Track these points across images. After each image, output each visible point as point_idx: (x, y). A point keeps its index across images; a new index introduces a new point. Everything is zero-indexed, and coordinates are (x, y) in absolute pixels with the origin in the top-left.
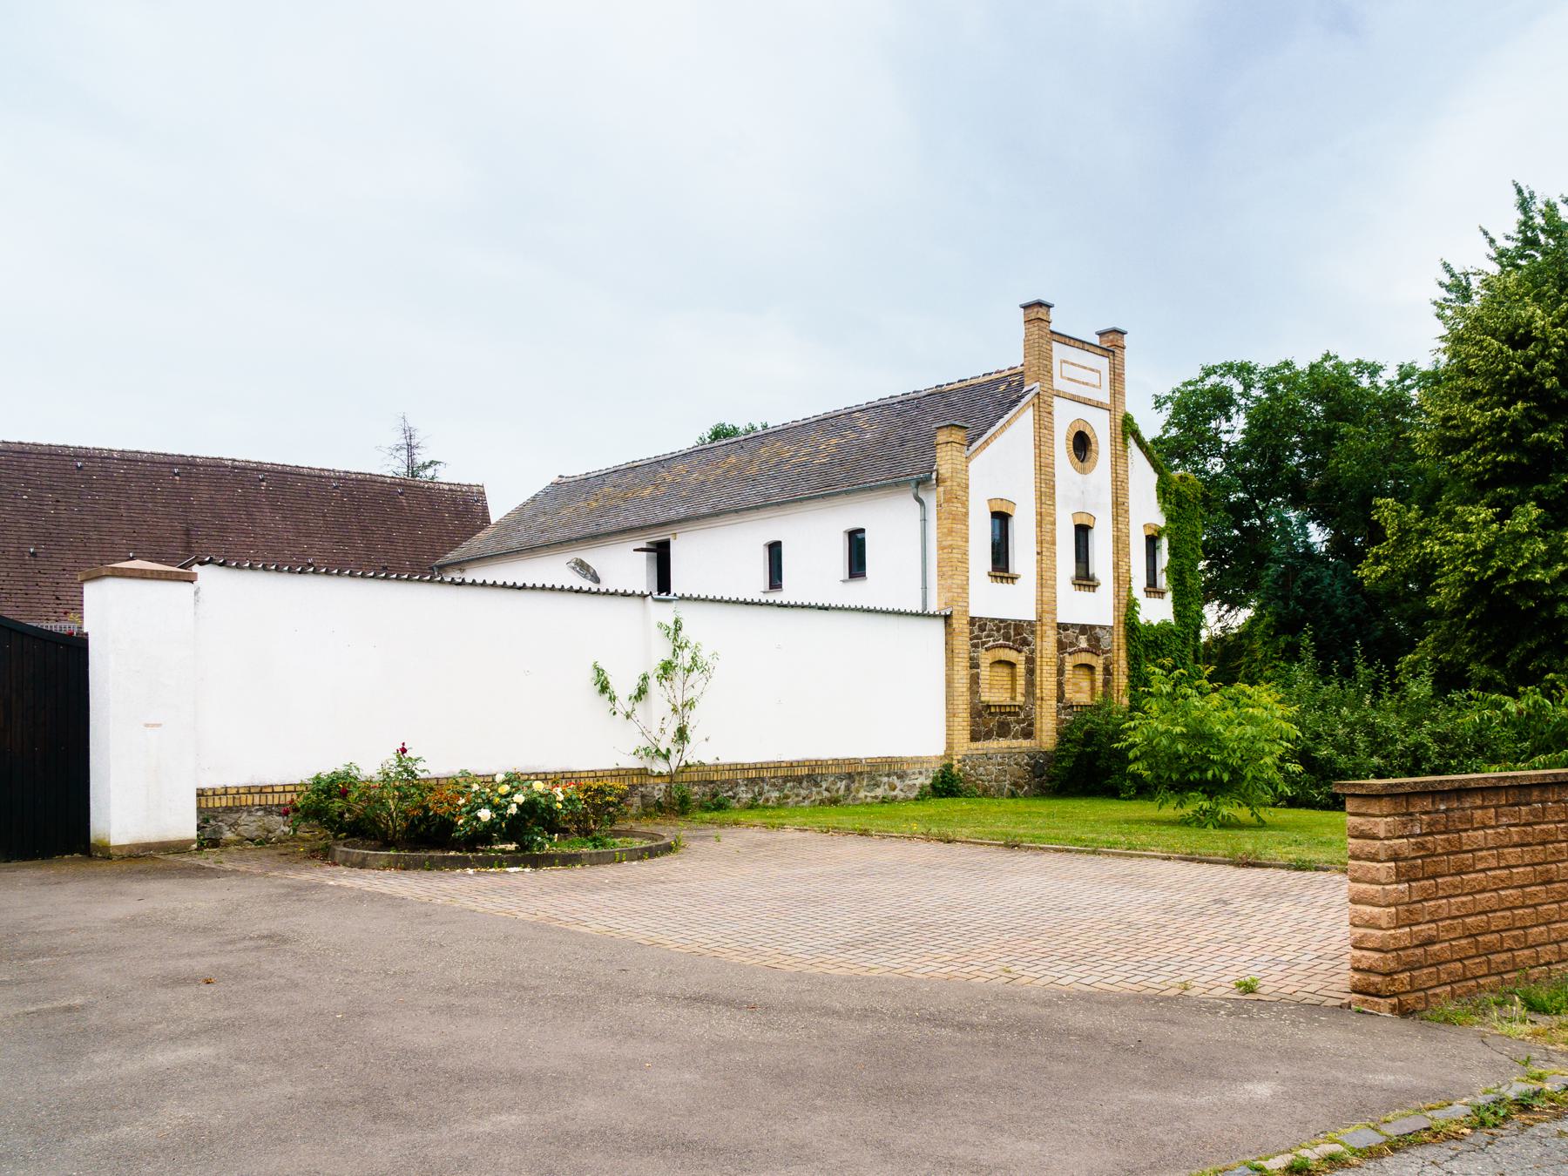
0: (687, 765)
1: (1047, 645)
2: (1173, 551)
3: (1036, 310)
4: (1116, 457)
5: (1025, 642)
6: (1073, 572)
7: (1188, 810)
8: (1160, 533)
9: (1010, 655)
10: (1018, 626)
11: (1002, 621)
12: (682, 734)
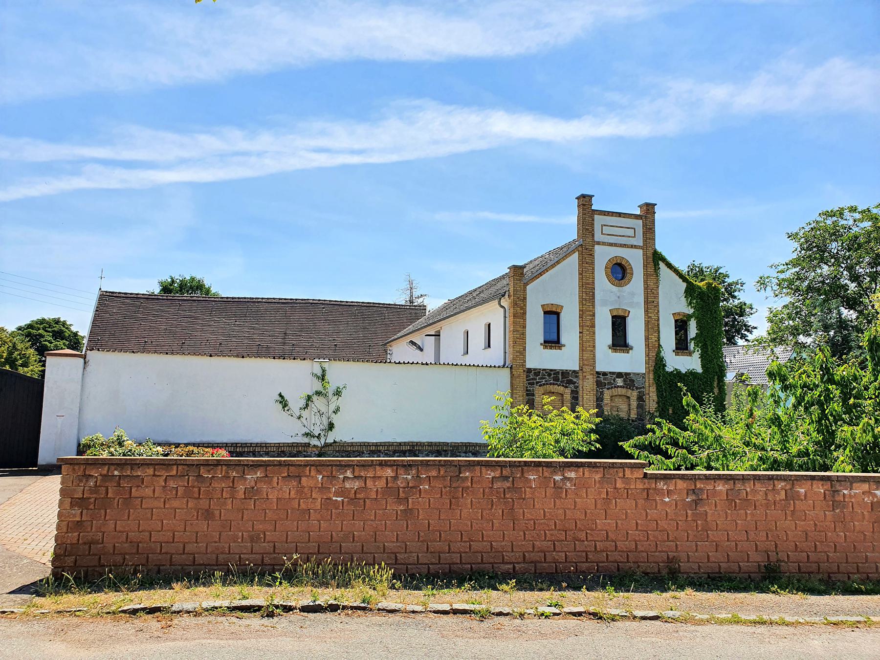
0: (335, 442)
1: (587, 386)
2: (699, 326)
3: (585, 201)
4: (647, 276)
5: (571, 382)
6: (610, 341)
7: (733, 401)
8: (689, 317)
9: (561, 389)
10: (565, 373)
11: (551, 370)
12: (331, 426)
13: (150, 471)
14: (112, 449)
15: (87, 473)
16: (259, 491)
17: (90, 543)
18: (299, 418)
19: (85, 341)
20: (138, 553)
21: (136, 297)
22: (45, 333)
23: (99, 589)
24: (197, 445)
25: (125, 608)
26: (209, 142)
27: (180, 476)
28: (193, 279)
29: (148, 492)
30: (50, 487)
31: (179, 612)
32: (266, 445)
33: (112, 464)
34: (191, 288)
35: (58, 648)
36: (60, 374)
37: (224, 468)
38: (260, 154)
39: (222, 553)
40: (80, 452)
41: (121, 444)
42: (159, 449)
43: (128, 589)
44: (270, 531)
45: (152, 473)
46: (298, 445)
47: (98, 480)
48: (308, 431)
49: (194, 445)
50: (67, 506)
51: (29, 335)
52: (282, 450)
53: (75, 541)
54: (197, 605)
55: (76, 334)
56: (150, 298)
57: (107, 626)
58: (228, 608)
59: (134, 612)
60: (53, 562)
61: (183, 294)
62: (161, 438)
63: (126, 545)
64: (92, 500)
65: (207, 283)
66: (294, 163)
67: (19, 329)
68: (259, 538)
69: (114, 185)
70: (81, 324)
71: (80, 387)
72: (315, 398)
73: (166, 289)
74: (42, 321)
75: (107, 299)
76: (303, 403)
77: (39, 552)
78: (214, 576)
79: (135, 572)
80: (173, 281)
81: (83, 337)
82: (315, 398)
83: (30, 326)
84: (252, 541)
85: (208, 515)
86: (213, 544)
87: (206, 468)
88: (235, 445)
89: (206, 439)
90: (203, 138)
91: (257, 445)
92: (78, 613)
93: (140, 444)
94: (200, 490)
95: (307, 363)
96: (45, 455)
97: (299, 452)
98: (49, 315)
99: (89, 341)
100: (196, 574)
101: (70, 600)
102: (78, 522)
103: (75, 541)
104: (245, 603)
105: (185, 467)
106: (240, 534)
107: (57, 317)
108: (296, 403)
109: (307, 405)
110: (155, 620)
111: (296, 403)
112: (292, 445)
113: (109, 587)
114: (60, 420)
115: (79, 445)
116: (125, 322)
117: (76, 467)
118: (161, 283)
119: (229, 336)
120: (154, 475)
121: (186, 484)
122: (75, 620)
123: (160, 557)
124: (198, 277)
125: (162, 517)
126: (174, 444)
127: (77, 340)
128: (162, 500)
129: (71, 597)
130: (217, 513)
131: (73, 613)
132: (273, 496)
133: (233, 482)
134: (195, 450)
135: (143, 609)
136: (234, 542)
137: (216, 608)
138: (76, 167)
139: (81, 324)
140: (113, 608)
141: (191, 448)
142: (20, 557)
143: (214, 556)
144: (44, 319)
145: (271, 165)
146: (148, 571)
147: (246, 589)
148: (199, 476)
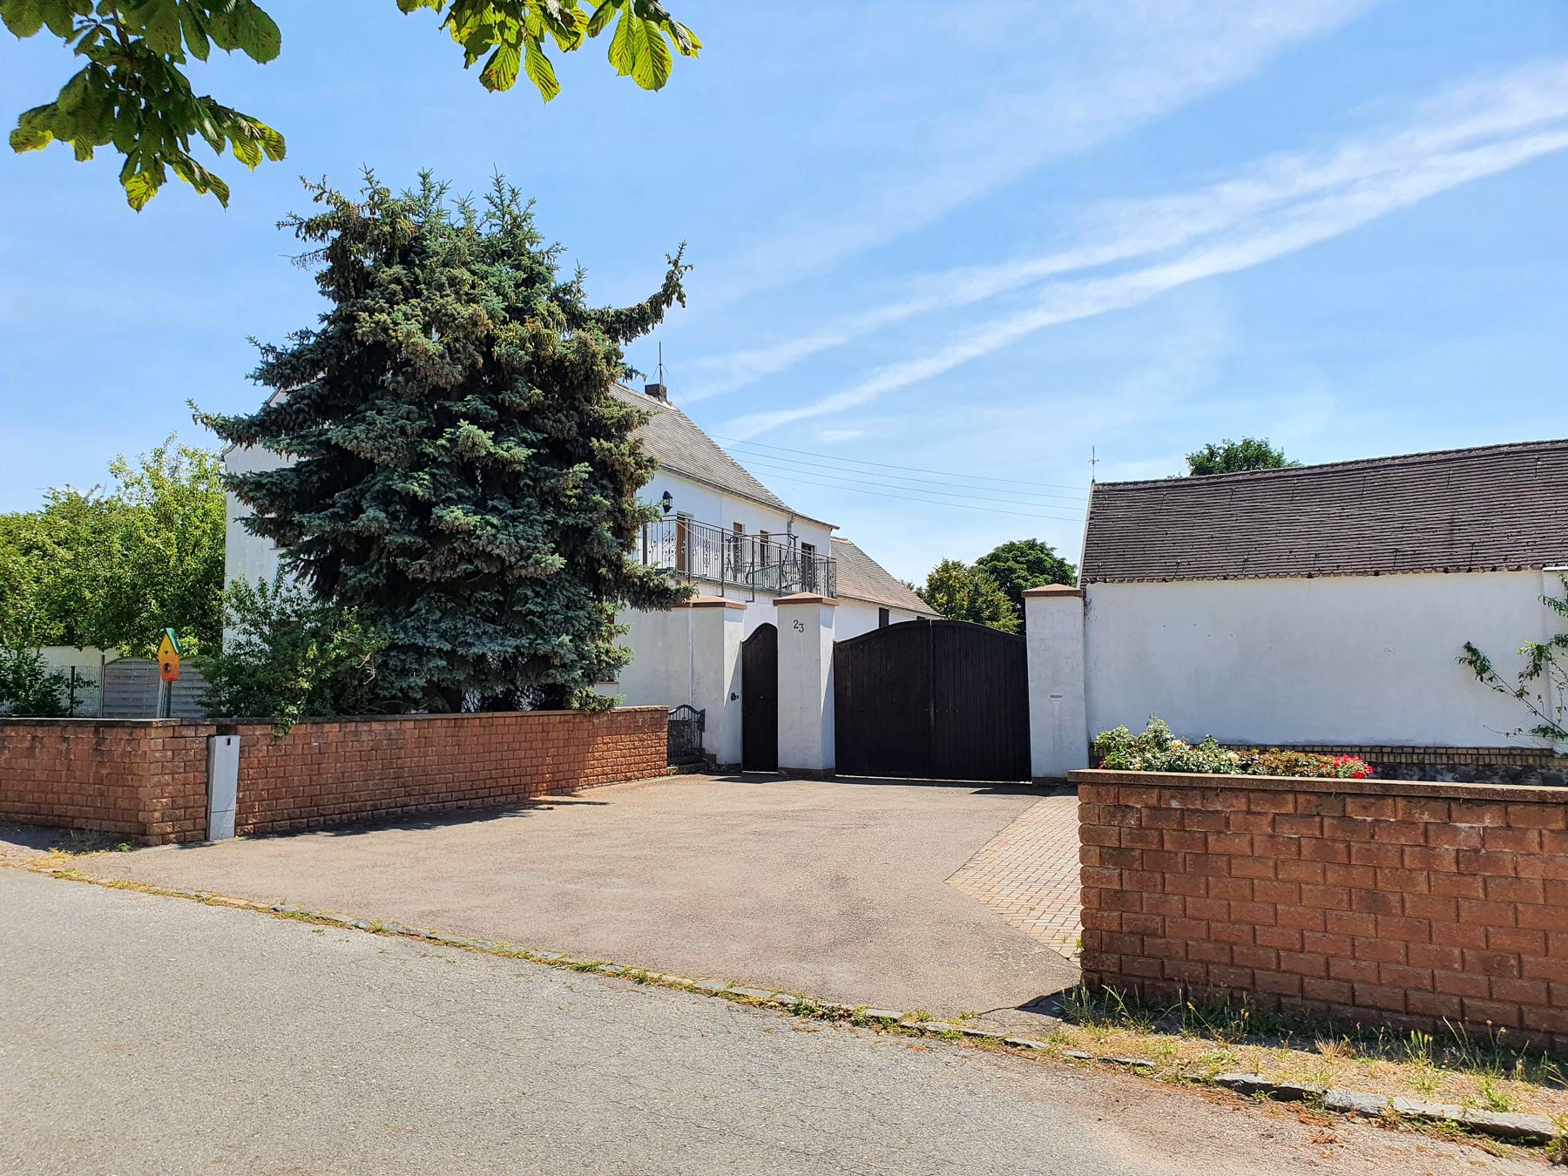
13: (1241, 803)
14: (1149, 755)
15: (1122, 802)
16: (1493, 861)
17: (1143, 934)
18: (1520, 694)
19: (1077, 573)
20: (1232, 964)
21: (1153, 487)
22: (1017, 566)
23: (1167, 1028)
24: (1305, 749)
25: (1228, 1077)
26: (1244, 194)
27: (1303, 816)
28: (1247, 444)
29: (1241, 844)
30: (1058, 819)
31: (1343, 1110)
32: (1448, 752)
33: (1169, 788)
34: (1247, 460)
35: (1111, 1141)
36: (1048, 623)
37: (1401, 803)
38: (1343, 189)
39: (1418, 989)
40: (1095, 761)
41: (1161, 744)
42: (1231, 755)
43: (1226, 1037)
44: (1534, 953)
45: (1244, 808)
46: (1523, 753)
47: (1145, 819)
48: (1544, 723)
49: (1294, 748)
50: (1095, 860)
51: (994, 570)
52: (1482, 763)
53: (1115, 927)
54: (1383, 1103)
55: (1061, 563)
56: (1175, 485)
57: (1197, 1111)
58: (1461, 1124)
59: (1247, 1089)
60: (1084, 957)
61: (1237, 470)
62: (1231, 736)
63: (1206, 945)
64: (1137, 853)
65: (1275, 448)
66: (1413, 188)
67: (981, 562)
68: (1503, 964)
69: (1089, 309)
70: (1069, 547)
71: (1081, 646)
72: (1556, 651)
73: (1202, 467)
74: (1011, 547)
75: (1106, 496)
76: (1526, 662)
77: (1057, 933)
78: (1408, 1038)
79: (1236, 1004)
80: (1212, 454)
81: (1074, 567)
82: (1556, 651)
83: (994, 557)
84: (1488, 971)
85: (1374, 902)
86: (1393, 967)
87: (1358, 801)
88: (1378, 750)
89: (1316, 738)
90: (1228, 189)
91: (1436, 751)
92: (1139, 1069)
93: (1194, 746)
94: (1349, 848)
95: (1527, 577)
96: (1042, 760)
97: (1531, 769)
98: (1019, 536)
99: (1085, 570)
100: (1371, 1027)
101: (1124, 1040)
102: (1116, 892)
103: (1115, 927)
104: (1499, 1119)
105: (1312, 798)
106: (1457, 952)
107: (1030, 538)
108: (1509, 661)
109: (1537, 669)
110: (1294, 1116)
111: (1509, 661)
112: (1511, 752)
113: (1188, 1025)
114: (1057, 702)
115: (1091, 746)
116: (1140, 530)
117: (1102, 790)
118: (1192, 460)
119: (1332, 538)
120: (1249, 812)
121: (1317, 834)
122: (1137, 1083)
123: (1278, 978)
124: (1257, 438)
125: (1279, 899)
126: (1257, 747)
127: (1065, 572)
128: (1271, 863)
129: (1123, 1033)
130: (1394, 899)
131: (1133, 1068)
132: (1533, 873)
133: (1426, 834)
134: (1302, 758)
135: (1266, 1088)
136: (1444, 967)
137: (1432, 1119)
138: (1030, 293)
139: (1068, 544)
140: (1203, 1073)
141: (1294, 755)
142: (1029, 942)
143: (1399, 993)
144: (1012, 544)
145: (1369, 204)
146: (1260, 1003)
147: (1499, 1087)
148: (1344, 817)
